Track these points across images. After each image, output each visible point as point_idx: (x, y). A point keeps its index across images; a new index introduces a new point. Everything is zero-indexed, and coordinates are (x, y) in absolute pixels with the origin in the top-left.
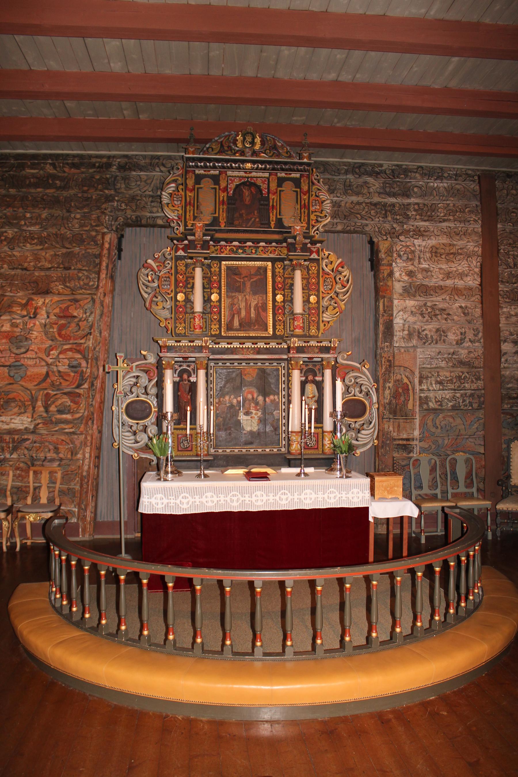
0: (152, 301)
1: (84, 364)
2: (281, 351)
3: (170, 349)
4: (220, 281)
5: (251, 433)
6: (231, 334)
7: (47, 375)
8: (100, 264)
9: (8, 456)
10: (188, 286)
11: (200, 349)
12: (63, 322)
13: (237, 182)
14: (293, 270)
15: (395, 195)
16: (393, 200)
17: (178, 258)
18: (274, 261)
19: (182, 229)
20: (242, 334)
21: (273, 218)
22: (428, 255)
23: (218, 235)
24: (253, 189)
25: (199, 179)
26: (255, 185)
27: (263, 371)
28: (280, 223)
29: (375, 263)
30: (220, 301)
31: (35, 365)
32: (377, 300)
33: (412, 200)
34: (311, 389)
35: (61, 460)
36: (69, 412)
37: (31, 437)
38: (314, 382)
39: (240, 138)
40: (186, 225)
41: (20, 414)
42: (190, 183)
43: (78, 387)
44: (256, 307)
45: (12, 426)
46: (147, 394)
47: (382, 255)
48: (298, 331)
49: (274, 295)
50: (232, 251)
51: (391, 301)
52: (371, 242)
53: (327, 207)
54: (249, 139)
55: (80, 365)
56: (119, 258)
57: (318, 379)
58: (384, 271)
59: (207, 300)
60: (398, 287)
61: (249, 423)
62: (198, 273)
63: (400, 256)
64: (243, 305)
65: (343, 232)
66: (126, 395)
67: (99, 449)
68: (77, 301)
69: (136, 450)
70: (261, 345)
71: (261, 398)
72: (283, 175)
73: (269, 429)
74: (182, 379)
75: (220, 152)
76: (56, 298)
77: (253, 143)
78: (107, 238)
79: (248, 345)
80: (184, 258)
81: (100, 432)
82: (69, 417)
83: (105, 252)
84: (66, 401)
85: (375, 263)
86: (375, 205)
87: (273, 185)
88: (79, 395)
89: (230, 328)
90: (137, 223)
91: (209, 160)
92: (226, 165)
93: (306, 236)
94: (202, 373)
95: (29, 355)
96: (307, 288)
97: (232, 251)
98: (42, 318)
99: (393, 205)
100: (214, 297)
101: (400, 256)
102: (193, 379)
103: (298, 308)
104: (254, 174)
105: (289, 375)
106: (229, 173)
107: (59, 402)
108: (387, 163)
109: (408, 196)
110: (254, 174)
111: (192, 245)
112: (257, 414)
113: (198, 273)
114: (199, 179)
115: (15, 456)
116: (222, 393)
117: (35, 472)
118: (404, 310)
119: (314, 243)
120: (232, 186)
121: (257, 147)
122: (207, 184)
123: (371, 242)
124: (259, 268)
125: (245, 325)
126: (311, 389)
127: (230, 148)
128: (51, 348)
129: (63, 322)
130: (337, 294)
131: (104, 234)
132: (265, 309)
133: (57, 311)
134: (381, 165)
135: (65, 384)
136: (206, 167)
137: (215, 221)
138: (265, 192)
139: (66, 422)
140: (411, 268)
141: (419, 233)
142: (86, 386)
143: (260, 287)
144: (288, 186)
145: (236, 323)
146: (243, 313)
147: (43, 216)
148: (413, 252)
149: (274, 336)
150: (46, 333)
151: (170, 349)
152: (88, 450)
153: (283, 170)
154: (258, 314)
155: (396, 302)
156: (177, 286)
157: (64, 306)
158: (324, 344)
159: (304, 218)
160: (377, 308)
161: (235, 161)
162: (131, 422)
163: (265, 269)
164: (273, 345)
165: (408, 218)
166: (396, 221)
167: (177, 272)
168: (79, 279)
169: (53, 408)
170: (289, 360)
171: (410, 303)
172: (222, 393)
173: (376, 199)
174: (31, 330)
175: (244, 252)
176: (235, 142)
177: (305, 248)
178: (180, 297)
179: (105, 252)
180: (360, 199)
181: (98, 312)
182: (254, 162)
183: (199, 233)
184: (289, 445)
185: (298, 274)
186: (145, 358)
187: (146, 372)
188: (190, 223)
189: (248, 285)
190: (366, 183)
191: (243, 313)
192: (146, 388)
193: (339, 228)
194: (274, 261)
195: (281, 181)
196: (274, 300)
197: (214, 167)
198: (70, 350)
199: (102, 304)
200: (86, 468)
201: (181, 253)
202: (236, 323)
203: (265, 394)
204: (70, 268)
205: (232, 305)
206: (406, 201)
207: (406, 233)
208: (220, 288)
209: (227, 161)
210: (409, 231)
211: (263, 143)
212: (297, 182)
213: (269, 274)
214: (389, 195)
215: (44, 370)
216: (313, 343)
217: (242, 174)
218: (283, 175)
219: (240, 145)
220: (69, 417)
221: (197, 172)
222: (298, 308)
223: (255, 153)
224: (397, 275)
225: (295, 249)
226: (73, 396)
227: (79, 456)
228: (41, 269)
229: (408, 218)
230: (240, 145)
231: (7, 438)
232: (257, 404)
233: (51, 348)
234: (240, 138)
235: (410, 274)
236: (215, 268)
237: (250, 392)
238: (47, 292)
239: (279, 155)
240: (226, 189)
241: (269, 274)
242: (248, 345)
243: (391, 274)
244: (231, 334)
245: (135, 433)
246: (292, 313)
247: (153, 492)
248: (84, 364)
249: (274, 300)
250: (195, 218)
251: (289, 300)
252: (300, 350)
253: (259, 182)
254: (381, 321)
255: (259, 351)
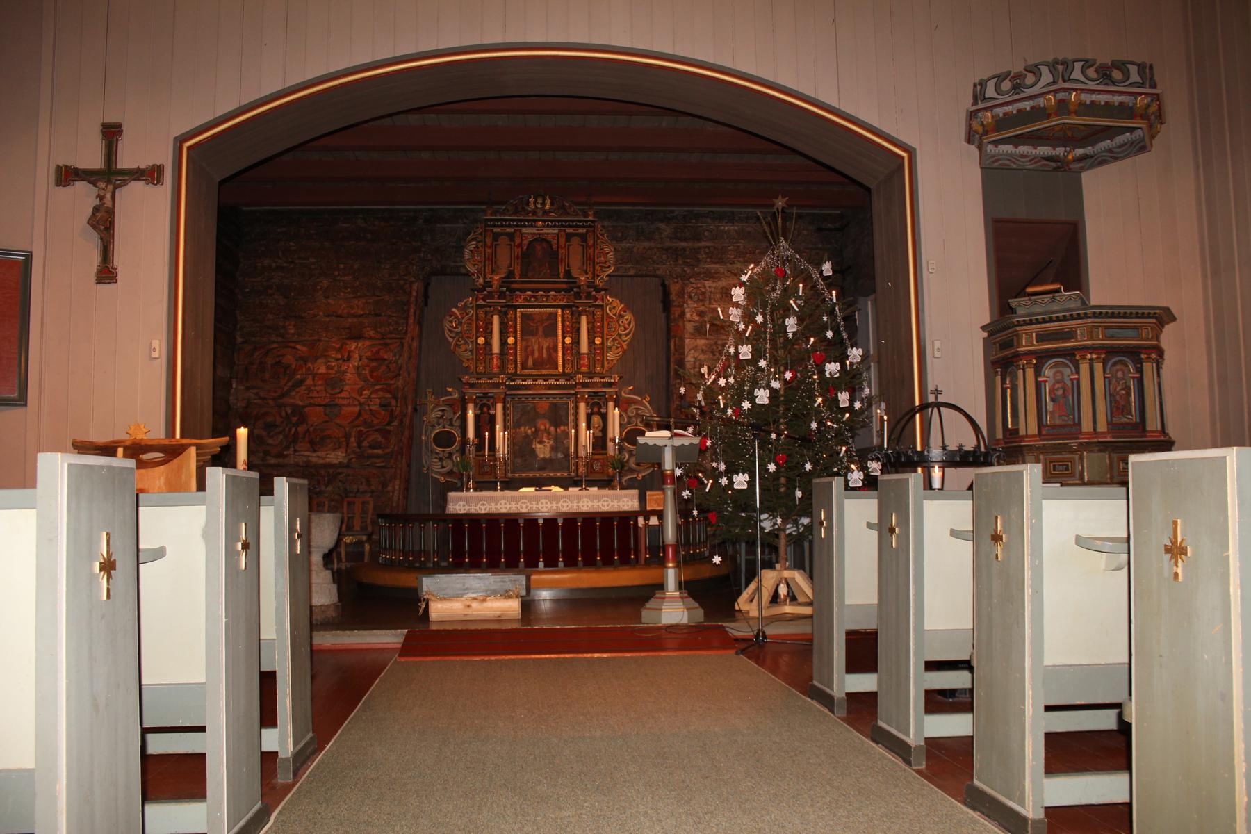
0: (457, 345)
1: (394, 403)
2: (571, 387)
3: (472, 385)
4: (515, 327)
5: (544, 459)
6: (526, 372)
7: (360, 414)
8: (408, 310)
9: (323, 488)
10: (488, 333)
11: (497, 385)
12: (374, 364)
13: (530, 238)
14: (580, 315)
15: (685, 239)
16: (684, 244)
17: (479, 307)
18: (563, 307)
19: (481, 280)
20: (535, 372)
21: (562, 270)
22: (718, 296)
23: (514, 286)
24: (545, 245)
25: (496, 237)
26: (545, 240)
27: (554, 405)
28: (568, 274)
29: (667, 305)
30: (515, 343)
31: (348, 405)
32: (669, 340)
33: (703, 244)
34: (596, 419)
35: (372, 492)
36: (380, 448)
37: (345, 470)
38: (599, 413)
39: (532, 200)
40: (485, 278)
41: (335, 449)
42: (489, 241)
43: (389, 424)
44: (548, 348)
45: (328, 460)
46: (451, 425)
47: (673, 297)
48: (584, 369)
49: (564, 338)
50: (525, 299)
51: (682, 340)
52: (664, 285)
53: (611, 257)
54: (540, 201)
55: (389, 405)
56: (426, 304)
57: (603, 411)
58: (676, 312)
59: (503, 342)
60: (689, 327)
61: (543, 450)
62: (496, 319)
63: (690, 297)
64: (536, 347)
65: (636, 276)
66: (433, 426)
67: (408, 481)
68: (387, 345)
69: (443, 475)
70: (552, 382)
71: (552, 429)
72: (570, 231)
73: (560, 455)
74: (482, 412)
75: (516, 213)
76: (368, 343)
77: (544, 204)
78: (415, 287)
79: (540, 382)
80: (484, 306)
81: (409, 465)
82: (380, 451)
83: (413, 299)
84: (378, 437)
85: (667, 305)
86: (667, 249)
87: (562, 241)
88: (389, 432)
89: (524, 367)
90: (443, 272)
91: (506, 220)
92: (519, 225)
93: (592, 285)
94: (499, 406)
95: (342, 395)
96: (592, 333)
97: (525, 299)
98: (355, 362)
99: (684, 249)
100: (511, 340)
101: (690, 297)
102: (492, 412)
103: (584, 348)
104: (545, 231)
105: (577, 408)
106: (524, 230)
107: (372, 438)
108: (678, 210)
109: (699, 240)
110: (545, 231)
111: (490, 295)
112: (549, 443)
113: (496, 319)
114: (496, 237)
115: (329, 488)
116: (517, 425)
117: (349, 503)
118: (695, 348)
119: (599, 291)
120: (526, 242)
121: (547, 207)
122: (504, 241)
123: (664, 285)
124: (550, 314)
125: (538, 364)
126: (596, 419)
127: (524, 209)
128: (363, 389)
129: (374, 364)
130: (620, 335)
131: (411, 283)
132: (556, 351)
133: (369, 354)
134: (673, 212)
135: (376, 421)
136: (502, 226)
137: (511, 274)
138: (555, 246)
139: (378, 456)
140: (702, 308)
141: (710, 275)
142: (395, 423)
143: (551, 331)
144: (576, 241)
145: (530, 363)
146: (536, 354)
147: (356, 267)
148: (703, 293)
149: (564, 374)
150: (359, 374)
151: (472, 385)
152: (397, 482)
153: (570, 226)
154: (549, 355)
155: (687, 341)
156: (477, 331)
157: (374, 350)
158: (606, 380)
159: (590, 269)
160: (668, 347)
161: (528, 221)
162: (438, 449)
163: (556, 314)
164: (562, 382)
165: (698, 260)
166: (686, 264)
167: (477, 319)
168: (389, 324)
169: (365, 444)
170: (575, 394)
171: (701, 342)
172: (517, 425)
173: (668, 244)
174: (344, 372)
175: (537, 300)
176: (528, 203)
177: (589, 296)
178: (481, 340)
179: (413, 299)
180: (652, 244)
181: (406, 355)
182: (544, 221)
183: (496, 284)
184: (577, 469)
185: (584, 319)
186: (450, 394)
187: (451, 405)
188: (488, 276)
189: (541, 329)
190: (658, 229)
191: (536, 354)
192: (451, 420)
193: (632, 273)
194: (563, 307)
195: (569, 237)
196: (563, 342)
197: (509, 226)
198: (381, 390)
199: (410, 347)
200: (395, 499)
201: (481, 302)
202: (530, 363)
203: (556, 425)
204: (379, 315)
205: (527, 347)
206: (697, 245)
207: (696, 275)
208: (515, 332)
209: (521, 221)
210: (699, 273)
211: (552, 204)
212: (583, 237)
213: (560, 319)
214: (681, 239)
215: (357, 409)
216: (598, 380)
217: (535, 231)
218: (570, 231)
219: (532, 206)
220: (380, 451)
221: (495, 230)
222: (584, 348)
223: (546, 213)
224: (688, 315)
225: (580, 298)
226: (385, 433)
227: (389, 488)
228: (354, 316)
229: (698, 260)
230: (532, 206)
231: (323, 472)
232: (549, 434)
233: (363, 389)
234: (532, 200)
235: (701, 314)
236: (511, 314)
237: (543, 424)
238: (359, 337)
239: (567, 214)
240: (520, 245)
241: (560, 319)
242: (540, 382)
243: (682, 315)
244: (526, 372)
245: (441, 460)
246: (578, 353)
247: (456, 501)
248: (394, 403)
249: (563, 342)
250: (493, 271)
251: (576, 341)
252: (584, 385)
253: (549, 238)
254: (672, 359)
255: (550, 387)
